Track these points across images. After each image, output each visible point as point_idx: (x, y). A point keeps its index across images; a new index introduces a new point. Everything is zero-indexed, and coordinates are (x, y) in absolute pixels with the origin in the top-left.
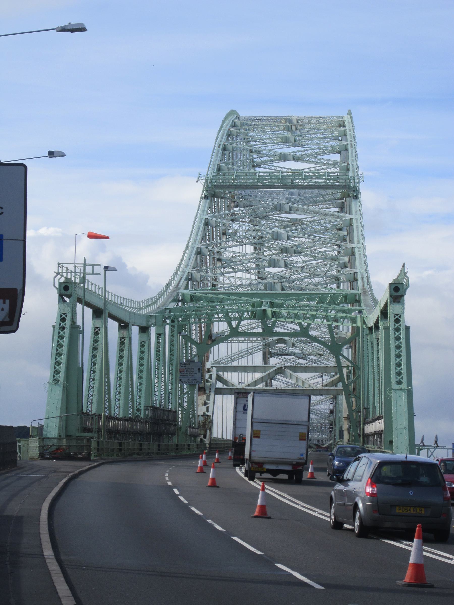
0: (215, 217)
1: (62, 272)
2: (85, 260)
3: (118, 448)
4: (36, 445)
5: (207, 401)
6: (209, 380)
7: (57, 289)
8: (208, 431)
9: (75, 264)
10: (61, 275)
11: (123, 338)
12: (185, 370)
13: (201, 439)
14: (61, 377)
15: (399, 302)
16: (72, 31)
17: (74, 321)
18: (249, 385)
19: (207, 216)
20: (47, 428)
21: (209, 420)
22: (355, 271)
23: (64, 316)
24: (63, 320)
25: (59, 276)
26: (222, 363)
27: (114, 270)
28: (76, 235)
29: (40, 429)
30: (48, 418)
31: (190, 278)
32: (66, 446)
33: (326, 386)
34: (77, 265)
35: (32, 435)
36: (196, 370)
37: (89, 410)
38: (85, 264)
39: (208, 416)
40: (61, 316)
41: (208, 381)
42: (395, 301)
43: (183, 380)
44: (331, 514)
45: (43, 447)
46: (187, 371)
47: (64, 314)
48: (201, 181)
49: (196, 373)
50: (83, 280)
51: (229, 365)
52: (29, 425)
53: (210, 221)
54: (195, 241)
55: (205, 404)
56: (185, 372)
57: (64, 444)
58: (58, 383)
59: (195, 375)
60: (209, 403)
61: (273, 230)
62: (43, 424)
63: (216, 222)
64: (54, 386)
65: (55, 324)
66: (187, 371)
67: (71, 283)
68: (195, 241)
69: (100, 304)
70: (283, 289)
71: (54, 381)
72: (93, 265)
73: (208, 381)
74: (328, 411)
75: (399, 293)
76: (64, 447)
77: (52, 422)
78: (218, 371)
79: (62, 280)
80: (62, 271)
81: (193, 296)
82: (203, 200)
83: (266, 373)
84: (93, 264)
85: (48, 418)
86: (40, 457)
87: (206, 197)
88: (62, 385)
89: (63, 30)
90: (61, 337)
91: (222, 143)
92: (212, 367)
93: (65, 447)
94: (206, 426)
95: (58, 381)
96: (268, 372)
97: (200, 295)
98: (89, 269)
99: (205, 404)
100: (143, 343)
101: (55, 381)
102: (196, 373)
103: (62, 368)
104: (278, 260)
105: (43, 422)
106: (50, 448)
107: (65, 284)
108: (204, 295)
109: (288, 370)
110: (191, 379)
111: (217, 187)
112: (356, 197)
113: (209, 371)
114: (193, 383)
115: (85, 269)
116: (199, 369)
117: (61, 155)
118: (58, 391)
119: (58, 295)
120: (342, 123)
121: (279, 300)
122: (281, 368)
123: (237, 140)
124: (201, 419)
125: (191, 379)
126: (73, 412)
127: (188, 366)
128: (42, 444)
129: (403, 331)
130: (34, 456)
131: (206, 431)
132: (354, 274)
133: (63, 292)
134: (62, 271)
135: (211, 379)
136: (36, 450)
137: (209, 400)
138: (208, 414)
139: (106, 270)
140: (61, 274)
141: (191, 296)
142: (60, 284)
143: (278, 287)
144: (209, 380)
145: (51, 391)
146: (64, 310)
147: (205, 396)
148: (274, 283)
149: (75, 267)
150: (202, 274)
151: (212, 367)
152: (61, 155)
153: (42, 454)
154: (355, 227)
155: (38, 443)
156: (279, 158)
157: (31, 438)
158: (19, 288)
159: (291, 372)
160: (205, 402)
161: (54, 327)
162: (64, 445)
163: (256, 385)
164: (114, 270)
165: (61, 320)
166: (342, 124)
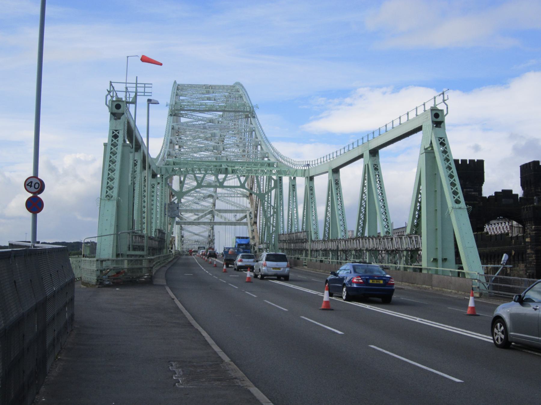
0: (177, 125)
3: (145, 245)
4: (92, 268)
7: (109, 107)
8: (174, 245)
13: (170, 250)
14: (115, 193)
15: (440, 127)
18: (195, 220)
19: (173, 124)
20: (101, 246)
21: (174, 239)
23: (116, 133)
24: (116, 137)
28: (128, 57)
29: (93, 246)
30: (102, 236)
31: (169, 155)
32: (128, 269)
33: (238, 220)
35: (85, 254)
36: (176, 209)
37: (379, 190)
39: (173, 237)
40: (113, 133)
42: (436, 127)
44: (124, 260)
45: (101, 271)
47: (116, 131)
49: (176, 210)
52: (83, 242)
53: (175, 127)
54: (168, 136)
57: (125, 267)
58: (112, 199)
61: (212, 131)
62: (96, 241)
64: (107, 202)
65: (107, 142)
68: (168, 136)
74: (207, 236)
75: (439, 120)
76: (126, 270)
77: (105, 240)
82: (169, 117)
85: (102, 236)
86: (98, 284)
87: (171, 115)
88: (116, 201)
90: (114, 153)
93: (127, 269)
96: (205, 213)
100: (153, 185)
101: (109, 197)
102: (176, 210)
103: (116, 184)
104: (219, 146)
105: (95, 240)
106: (109, 271)
109: (216, 212)
111: (177, 110)
114: (174, 216)
115: (136, 90)
118: (111, 206)
119: (110, 113)
126: (125, 228)
128: (100, 268)
130: (90, 282)
131: (172, 245)
133: (115, 110)
136: (91, 274)
139: (149, 102)
141: (174, 163)
145: (104, 207)
146: (116, 127)
153: (101, 280)
155: (95, 266)
156: (206, 99)
157: (84, 259)
159: (218, 213)
161: (105, 145)
162: (126, 268)
163: (198, 220)
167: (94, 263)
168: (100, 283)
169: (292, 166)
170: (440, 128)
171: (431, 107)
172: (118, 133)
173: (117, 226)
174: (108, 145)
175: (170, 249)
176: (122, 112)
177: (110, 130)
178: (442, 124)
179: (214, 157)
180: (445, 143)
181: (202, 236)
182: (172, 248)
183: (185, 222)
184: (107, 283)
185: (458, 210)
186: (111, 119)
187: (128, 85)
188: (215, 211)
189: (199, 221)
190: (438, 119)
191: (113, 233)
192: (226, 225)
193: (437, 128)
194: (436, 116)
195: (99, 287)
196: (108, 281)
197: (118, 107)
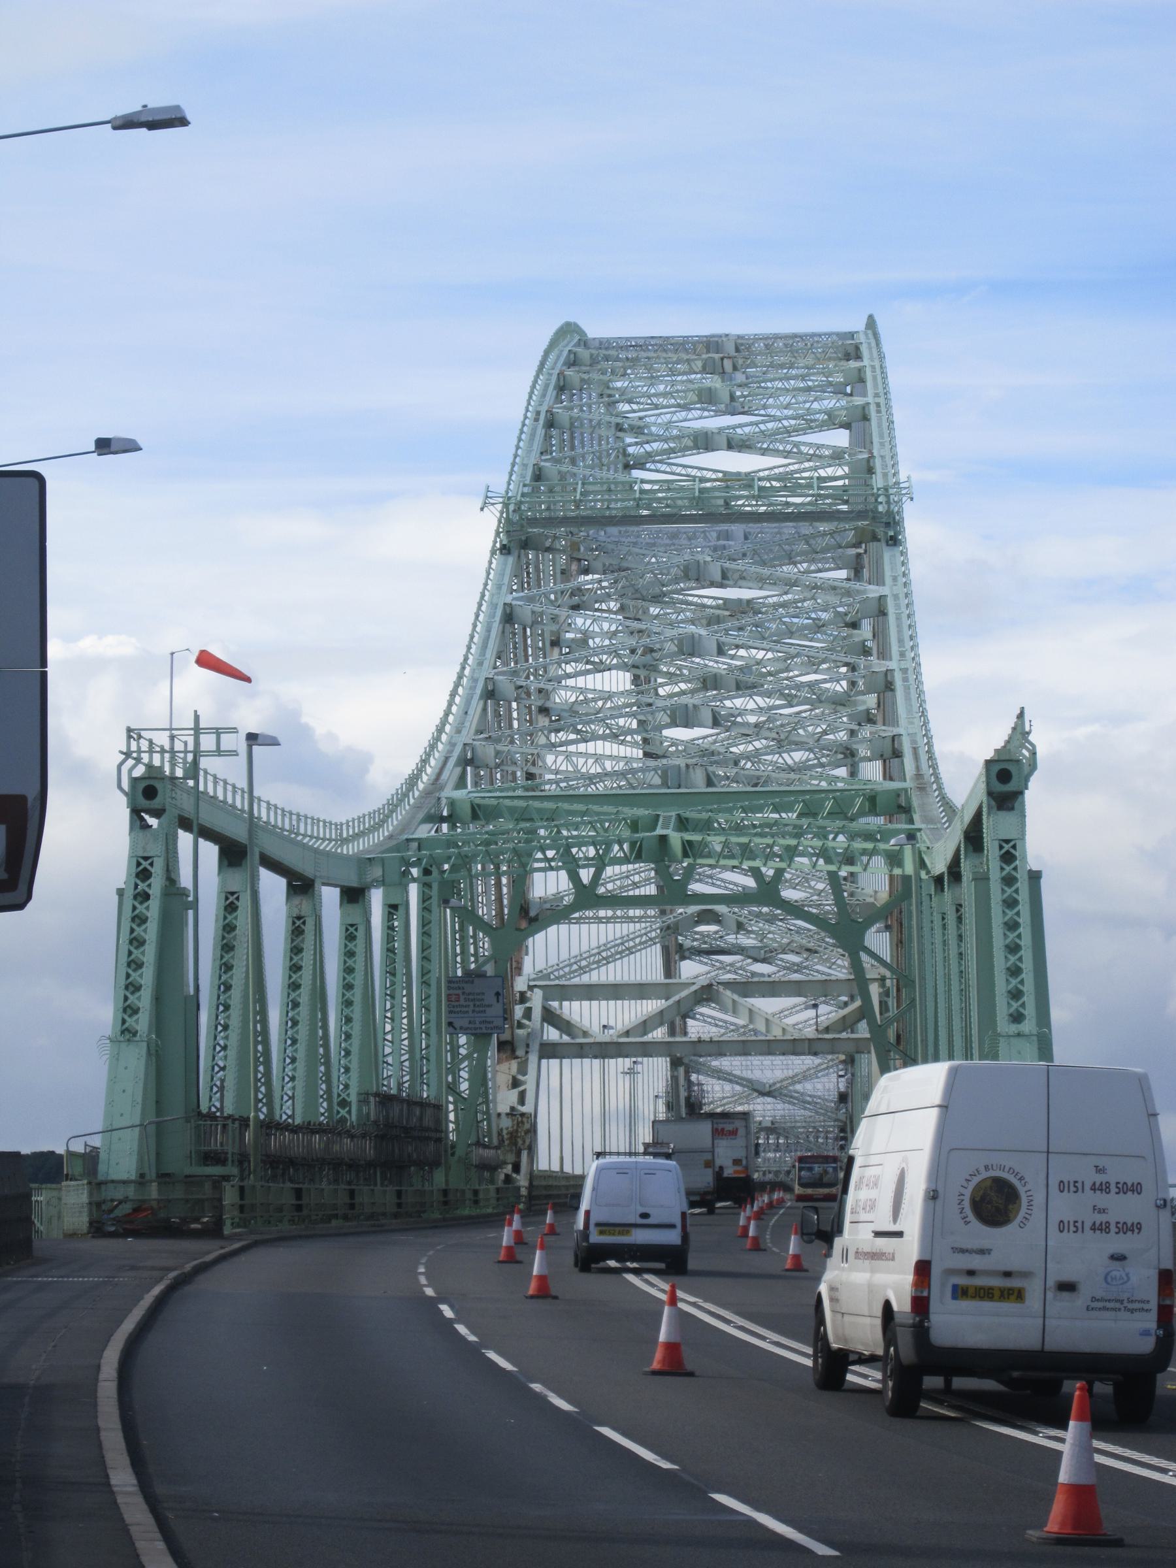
0: (530, 600)
1: (139, 751)
2: (197, 718)
5: (520, 1077)
6: (525, 1022)
8: (525, 1154)
9: (171, 729)
10: (135, 759)
11: (299, 918)
12: (462, 998)
14: (142, 1023)
16: (152, 125)
17: (173, 876)
18: (627, 1033)
19: (509, 599)
21: (527, 1126)
22: (896, 731)
23: (145, 864)
24: (144, 874)
25: (131, 762)
26: (557, 978)
27: (274, 742)
28: (172, 654)
29: (91, 1159)
32: (159, 1201)
33: (827, 1030)
34: (175, 732)
36: (490, 998)
38: (197, 730)
39: (523, 1115)
40: (139, 864)
41: (520, 1026)
43: (457, 1024)
46: (466, 1000)
47: (146, 858)
48: (491, 507)
49: (490, 1006)
50: (193, 770)
51: (576, 981)
53: (518, 611)
55: (515, 1083)
56: (462, 1002)
59: (487, 1009)
60: (523, 1083)
63: (533, 612)
64: (123, 1045)
65: (123, 886)
66: (466, 1000)
67: (163, 779)
69: (238, 832)
70: (710, 783)
71: (123, 1032)
72: (218, 732)
73: (520, 1026)
74: (834, 1096)
76: (154, 1204)
78: (546, 998)
79: (139, 771)
80: (139, 747)
81: (479, 806)
83: (671, 1002)
84: (217, 729)
86: (92, 1230)
87: (505, 550)
88: (145, 1044)
89: (126, 123)
90: (139, 920)
91: (544, 409)
92: (531, 988)
94: (520, 1142)
95: (135, 1034)
96: (676, 998)
97: (494, 802)
98: (208, 742)
99: (515, 1083)
101: (126, 1033)
102: (490, 1006)
105: (96, 1141)
106: (117, 1206)
107: (147, 783)
108: (507, 802)
109: (728, 993)
110: (477, 1020)
111: (533, 522)
112: (894, 541)
113: (523, 998)
114: (485, 1031)
116: (498, 994)
117: (130, 447)
118: (136, 1058)
120: (851, 350)
121: (700, 812)
122: (710, 986)
123: (581, 399)
124: (506, 1123)
125: (477, 1020)
127: (468, 988)
129: (1023, 885)
132: (893, 738)
133: (143, 802)
134: (139, 747)
135: (529, 1019)
137: (525, 1074)
138: (523, 1109)
140: (135, 755)
142: (134, 781)
143: (698, 777)
144: (525, 1022)
145: (118, 1059)
146: (145, 850)
147: (514, 1065)
148: (687, 766)
149: (172, 738)
150: (499, 747)
151: (531, 988)
152: (130, 447)
153: (98, 1222)
154: (892, 618)
156: (690, 444)
158: (32, 794)
159: (736, 997)
160: (514, 1078)
161: (120, 893)
162: (154, 1200)
163: (645, 1033)
164: (274, 742)
165: (137, 875)
166: (853, 354)
167: (84, 1189)
168: (97, 1229)
169: (946, 819)
170: (1011, 813)
171: (996, 750)
172: (151, 864)
173: (157, 1102)
174: (126, 892)
175: (509, 1169)
176: (160, 807)
177: (131, 857)
178: (1020, 797)
179: (655, 770)
180: (1017, 854)
181: (801, 1100)
182: (517, 1168)
183: (581, 1045)
184: (113, 1229)
185: (1014, 1041)
186: (132, 829)
187: (175, 732)
188: (721, 988)
189: (645, 1039)
190: (1009, 785)
191: (138, 1123)
192: (746, 1053)
193: (1002, 814)
194: (1004, 776)
195: (93, 1237)
196: (113, 1225)
197: (150, 792)
